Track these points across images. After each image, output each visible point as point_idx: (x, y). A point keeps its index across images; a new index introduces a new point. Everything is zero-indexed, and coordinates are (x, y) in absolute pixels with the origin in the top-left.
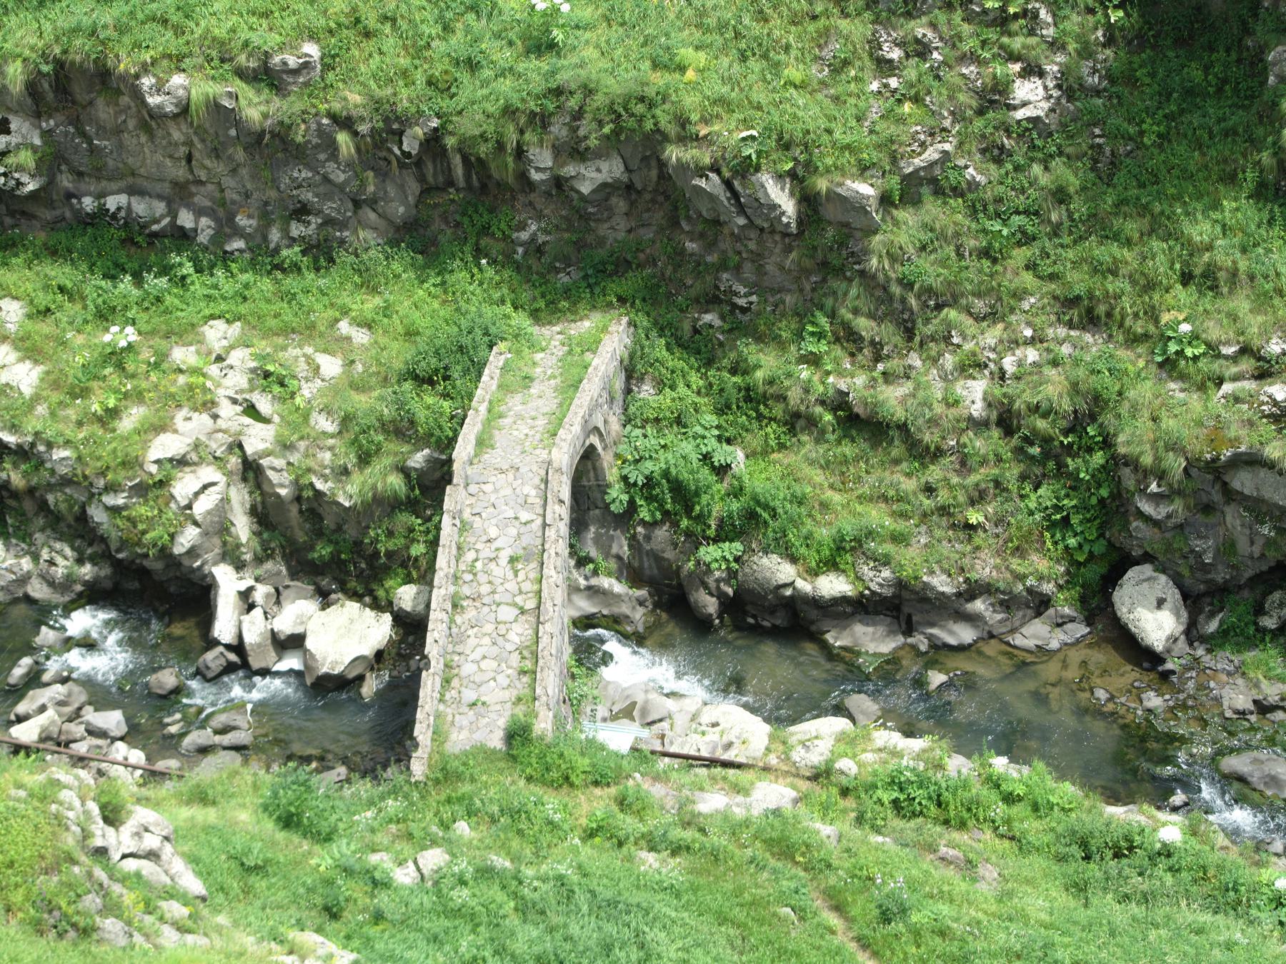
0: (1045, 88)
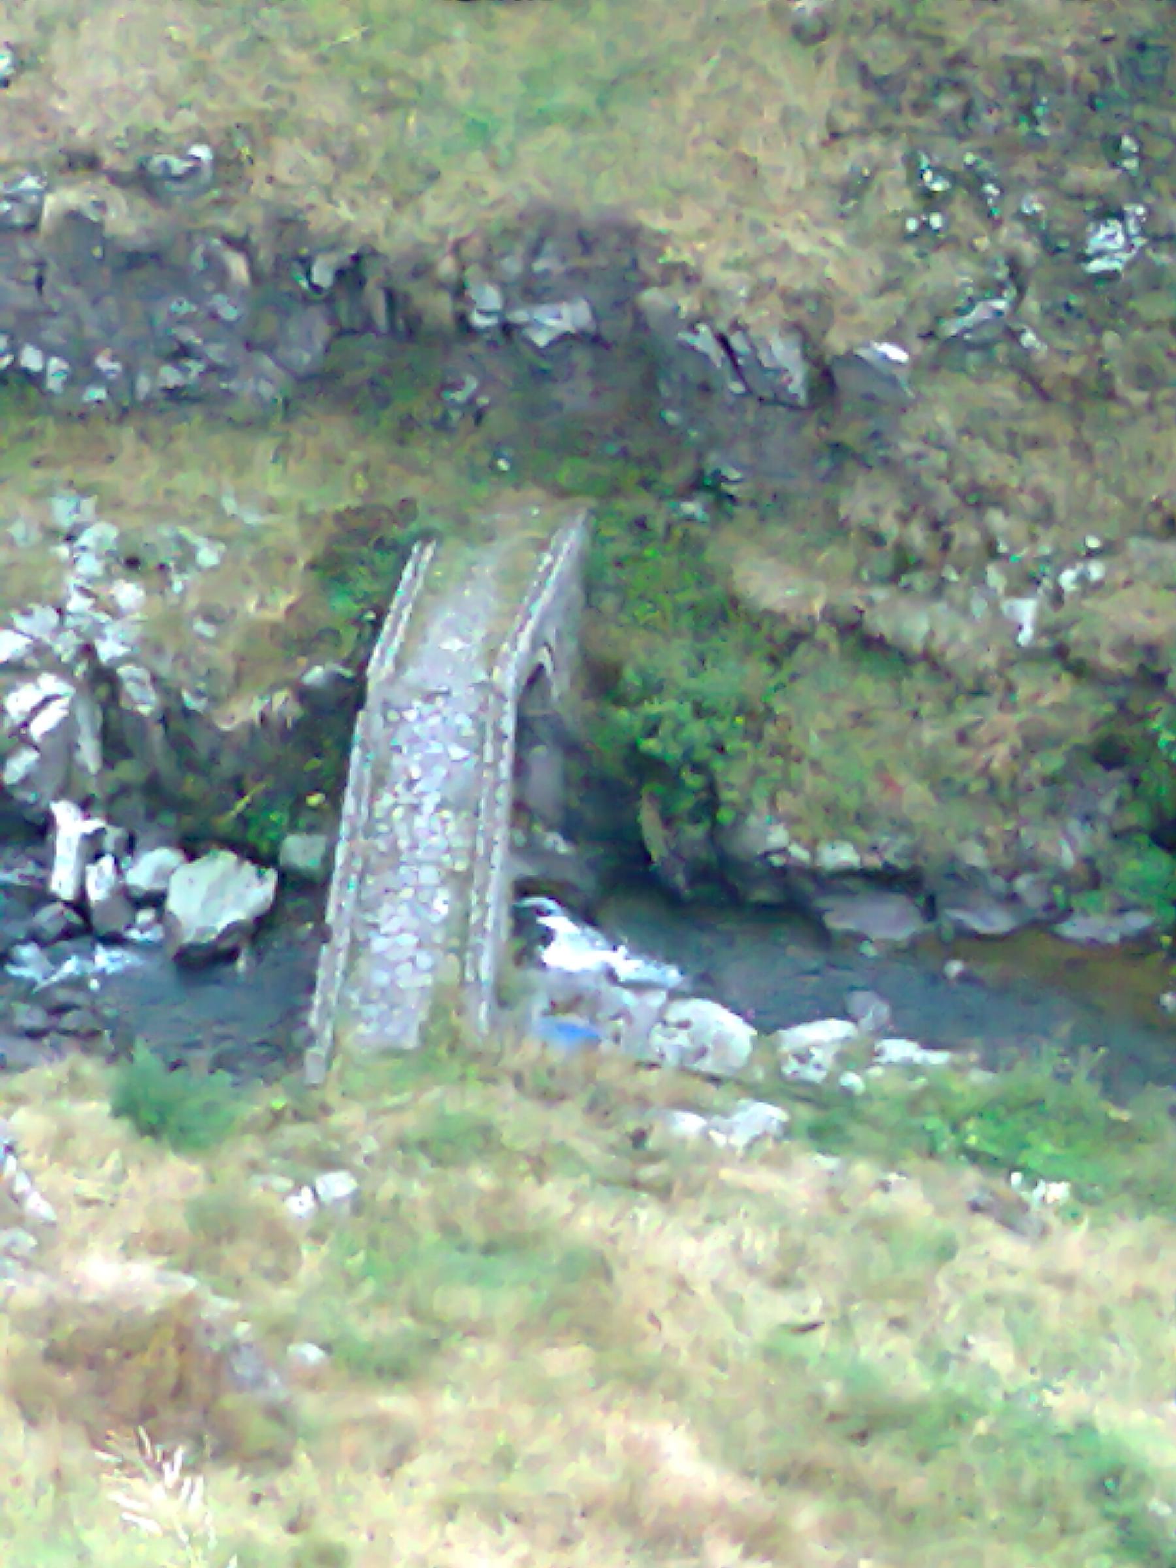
0: (1128, 237)
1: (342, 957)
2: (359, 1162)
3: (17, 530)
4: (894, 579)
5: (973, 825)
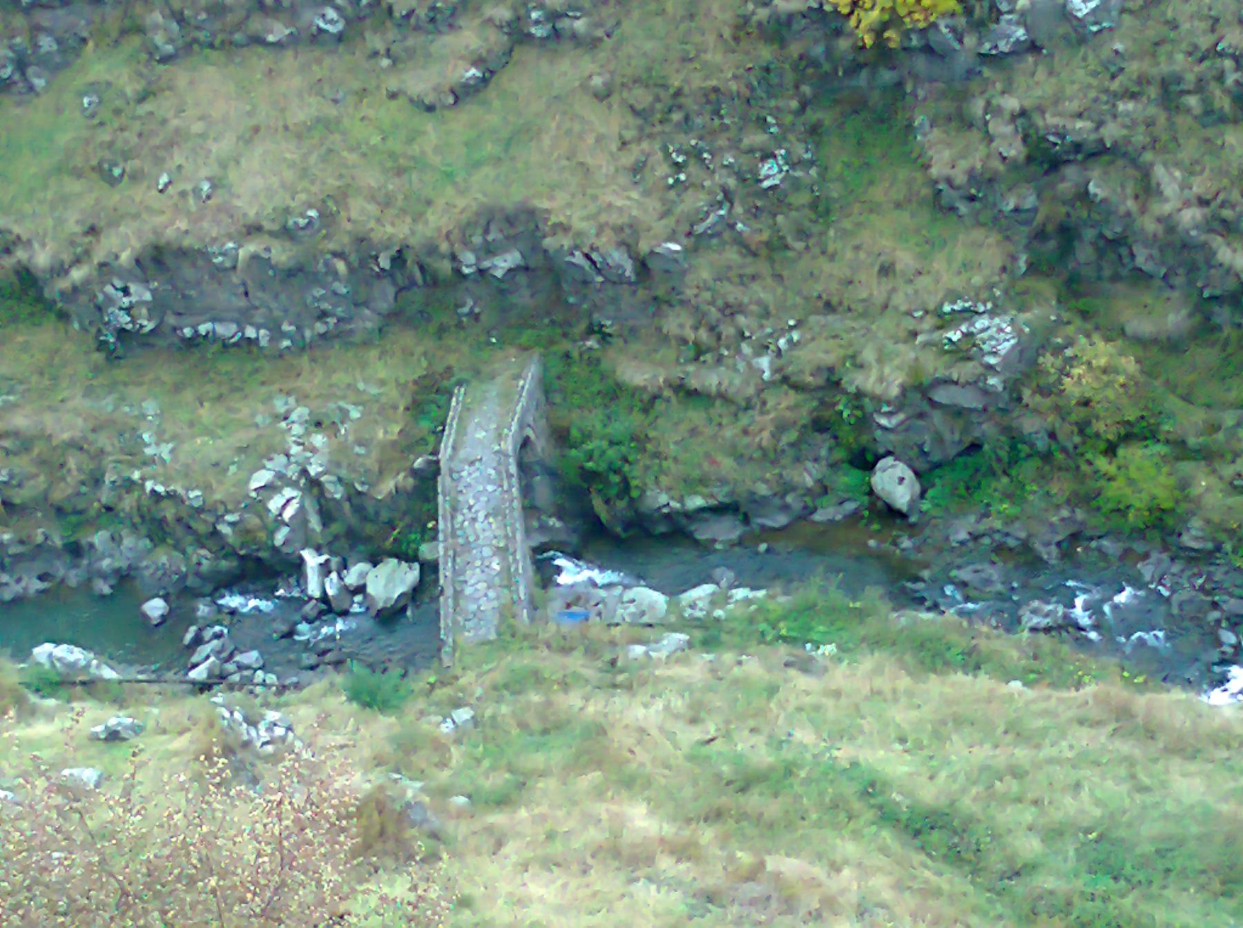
1: (450, 601)
2: (473, 701)
3: (259, 419)
4: (696, 359)
5: (758, 474)
